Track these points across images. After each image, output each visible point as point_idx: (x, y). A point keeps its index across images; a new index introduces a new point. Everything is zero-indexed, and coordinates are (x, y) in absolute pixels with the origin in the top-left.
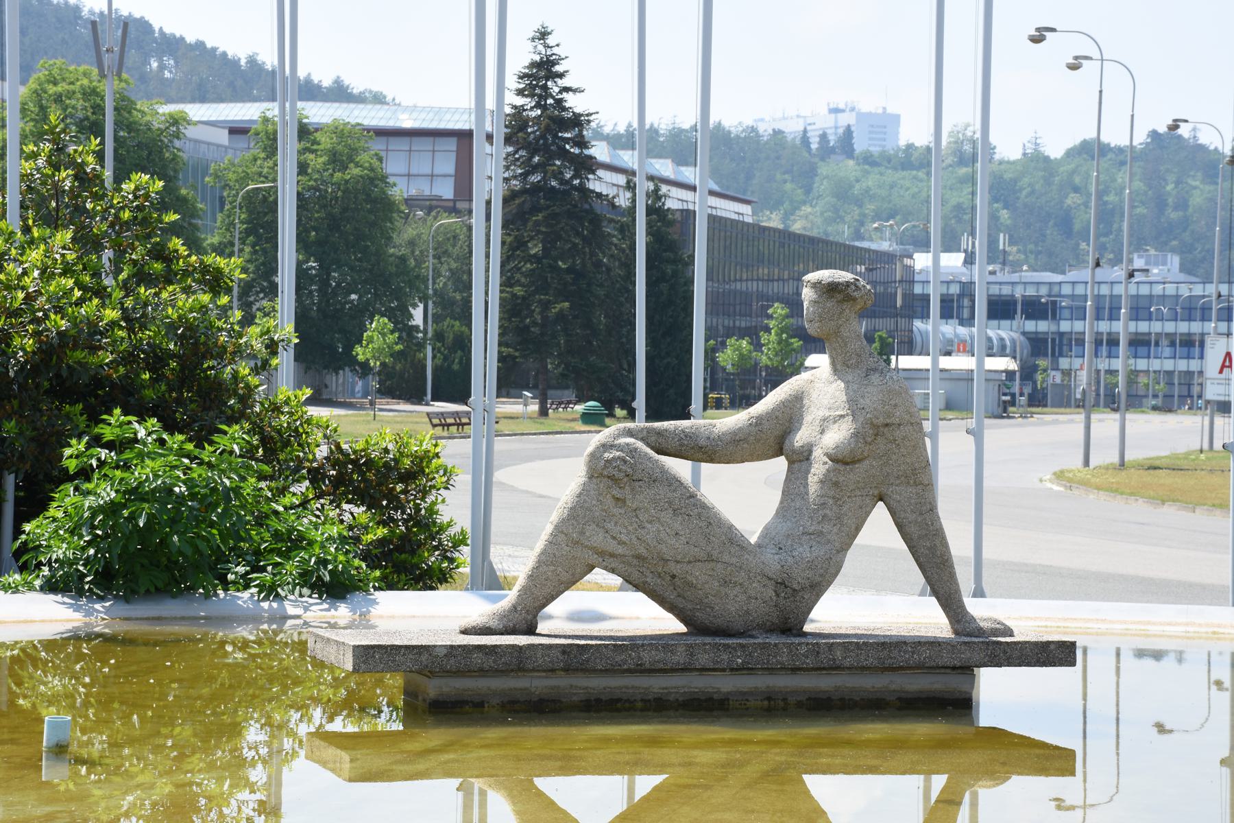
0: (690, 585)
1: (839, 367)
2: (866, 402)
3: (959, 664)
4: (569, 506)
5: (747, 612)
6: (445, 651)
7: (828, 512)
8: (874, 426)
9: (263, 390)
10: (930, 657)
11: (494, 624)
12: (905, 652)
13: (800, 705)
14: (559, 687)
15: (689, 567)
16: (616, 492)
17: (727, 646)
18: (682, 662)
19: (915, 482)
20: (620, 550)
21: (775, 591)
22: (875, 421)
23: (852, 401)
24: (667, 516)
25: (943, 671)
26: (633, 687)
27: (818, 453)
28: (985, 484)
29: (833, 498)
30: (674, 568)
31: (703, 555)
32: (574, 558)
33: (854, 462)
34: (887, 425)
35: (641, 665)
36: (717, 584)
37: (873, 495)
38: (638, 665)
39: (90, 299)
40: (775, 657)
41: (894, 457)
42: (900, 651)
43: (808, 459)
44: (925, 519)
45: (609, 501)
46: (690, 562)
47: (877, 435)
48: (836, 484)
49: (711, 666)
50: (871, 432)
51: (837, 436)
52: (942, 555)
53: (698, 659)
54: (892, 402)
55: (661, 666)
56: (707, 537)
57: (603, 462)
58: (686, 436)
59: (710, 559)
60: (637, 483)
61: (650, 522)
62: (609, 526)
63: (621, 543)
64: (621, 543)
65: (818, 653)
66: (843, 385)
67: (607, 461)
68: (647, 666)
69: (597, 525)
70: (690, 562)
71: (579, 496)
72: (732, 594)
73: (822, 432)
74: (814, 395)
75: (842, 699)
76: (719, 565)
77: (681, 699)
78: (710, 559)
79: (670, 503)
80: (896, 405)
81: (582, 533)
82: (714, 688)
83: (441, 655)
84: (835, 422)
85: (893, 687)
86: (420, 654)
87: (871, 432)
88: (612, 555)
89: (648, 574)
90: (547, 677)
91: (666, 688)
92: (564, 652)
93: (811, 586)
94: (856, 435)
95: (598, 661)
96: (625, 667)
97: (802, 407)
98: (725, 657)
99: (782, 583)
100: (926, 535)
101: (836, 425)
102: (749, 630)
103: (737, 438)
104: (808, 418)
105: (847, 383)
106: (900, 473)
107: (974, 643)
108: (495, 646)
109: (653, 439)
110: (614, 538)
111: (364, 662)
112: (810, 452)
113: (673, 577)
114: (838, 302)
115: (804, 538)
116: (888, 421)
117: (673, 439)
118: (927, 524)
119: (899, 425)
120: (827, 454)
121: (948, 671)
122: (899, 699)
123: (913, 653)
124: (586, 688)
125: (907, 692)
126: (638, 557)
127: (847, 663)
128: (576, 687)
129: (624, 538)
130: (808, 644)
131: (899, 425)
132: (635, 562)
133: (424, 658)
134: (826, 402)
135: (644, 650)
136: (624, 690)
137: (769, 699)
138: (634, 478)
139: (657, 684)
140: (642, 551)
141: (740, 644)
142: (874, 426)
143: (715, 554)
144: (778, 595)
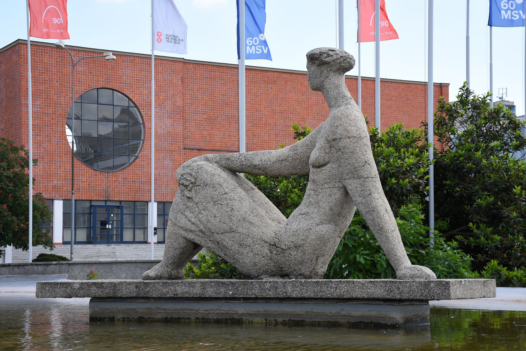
3: (366, 297)
6: (78, 286)
7: (311, 199)
8: (329, 142)
10: (347, 291)
12: (331, 288)
13: (284, 323)
14: (151, 309)
16: (187, 193)
17: (223, 283)
18: (198, 293)
19: (358, 176)
20: (193, 228)
21: (270, 250)
25: (377, 302)
26: (189, 309)
28: (108, 160)
29: (314, 190)
30: (218, 237)
31: (227, 228)
34: (334, 140)
35: (176, 295)
36: (237, 246)
37: (338, 187)
38: (174, 295)
40: (251, 290)
41: (342, 161)
42: (328, 287)
44: (367, 201)
46: (222, 233)
47: (331, 147)
49: (214, 295)
50: (328, 145)
52: (379, 225)
53: (207, 292)
54: (335, 125)
55: (187, 295)
56: (230, 217)
58: (245, 160)
60: (198, 187)
61: (204, 210)
64: (193, 223)
65: (277, 288)
69: (182, 214)
70: (222, 233)
72: (245, 252)
77: (215, 317)
78: (232, 231)
79: (212, 198)
80: (337, 126)
81: (176, 219)
82: (234, 311)
83: (77, 288)
85: (343, 313)
86: (67, 287)
87: (328, 145)
90: (145, 303)
91: (207, 310)
92: (137, 287)
93: (295, 247)
95: (154, 292)
96: (168, 296)
98: (222, 290)
99: (274, 245)
100: (369, 211)
102: (260, 275)
103: (281, 159)
106: (348, 171)
107: (377, 282)
109: (224, 162)
110: (189, 221)
111: (41, 292)
114: (318, 66)
116: (334, 137)
117: (237, 161)
118: (368, 204)
119: (340, 139)
121: (382, 303)
123: (336, 288)
124: (165, 309)
125: (352, 317)
127: (294, 295)
128: (160, 308)
129: (193, 220)
130: (270, 282)
131: (340, 139)
135: (178, 285)
136: (185, 311)
138: (197, 184)
139: (202, 308)
140: (202, 227)
141: (231, 282)
143: (234, 227)
144: (271, 252)
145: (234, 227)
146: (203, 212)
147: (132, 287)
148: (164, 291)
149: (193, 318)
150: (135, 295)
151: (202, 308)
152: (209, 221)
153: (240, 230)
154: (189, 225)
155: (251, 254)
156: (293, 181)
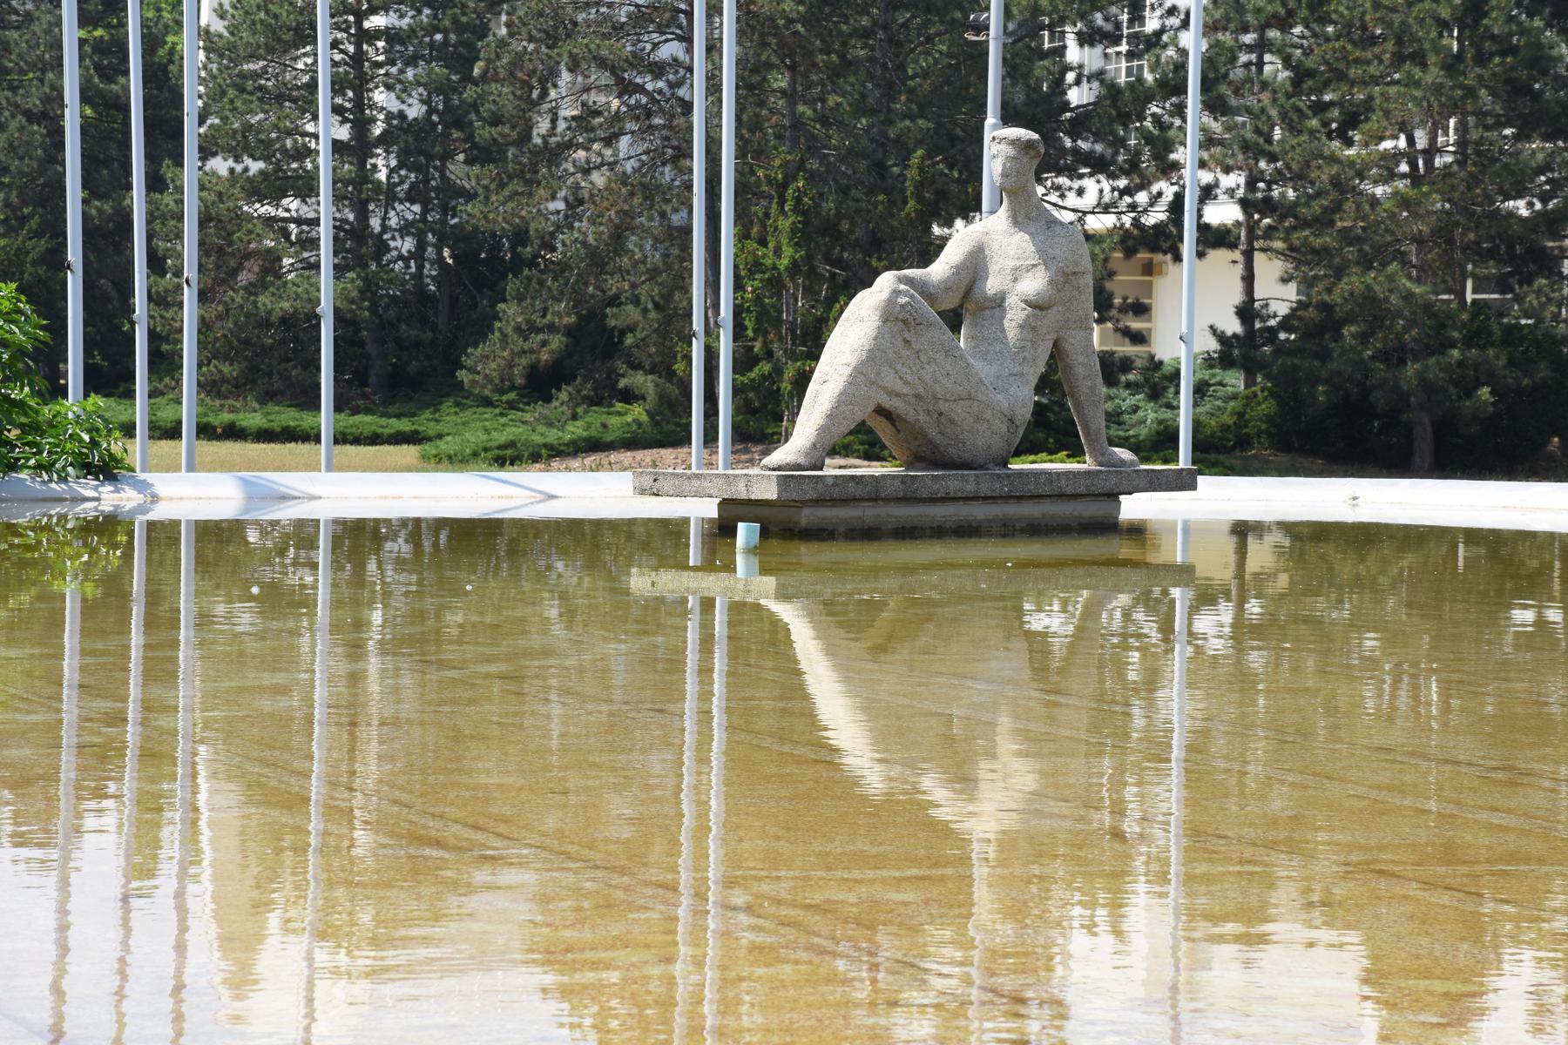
0: (952, 422)
1: (1020, 219)
2: (1056, 252)
4: (867, 348)
5: (989, 447)
8: (1065, 274)
9: (1475, 291)
11: (801, 460)
15: (953, 405)
20: (905, 390)
22: (1066, 270)
23: (1041, 252)
24: (940, 357)
27: (1012, 300)
30: (943, 406)
31: (964, 394)
32: (870, 397)
33: (1047, 309)
39: (344, 121)
43: (1000, 306)
45: (900, 343)
48: (1034, 328)
51: (1034, 283)
57: (898, 308)
59: (970, 398)
62: (899, 367)
63: (907, 383)
64: (907, 383)
66: (1027, 237)
67: (902, 306)
68: (952, 495)
71: (875, 338)
73: (1015, 280)
74: (995, 247)
75: (1046, 525)
76: (976, 404)
81: (878, 374)
84: (1028, 271)
85: (1076, 513)
88: (898, 395)
89: (921, 413)
92: (903, 482)
94: (1051, 282)
97: (985, 257)
101: (1030, 274)
104: (993, 268)
105: (1031, 234)
108: (862, 476)
110: (901, 378)
112: (1003, 299)
113: (941, 414)
115: (1012, 379)
120: (1026, 302)
122: (1079, 524)
126: (917, 396)
127: (1068, 492)
132: (914, 400)
133: (820, 486)
134: (1012, 252)
137: (1005, 525)
139: (940, 512)
140: (921, 391)
142: (1065, 274)
145: (972, 391)
146: (927, 367)
147: (897, 483)
148: (936, 487)
149: (842, 529)
150: (901, 494)
151: (940, 512)
152: (936, 381)
153: (979, 396)
154: (900, 387)
155: (988, 433)
156: (750, 333)
